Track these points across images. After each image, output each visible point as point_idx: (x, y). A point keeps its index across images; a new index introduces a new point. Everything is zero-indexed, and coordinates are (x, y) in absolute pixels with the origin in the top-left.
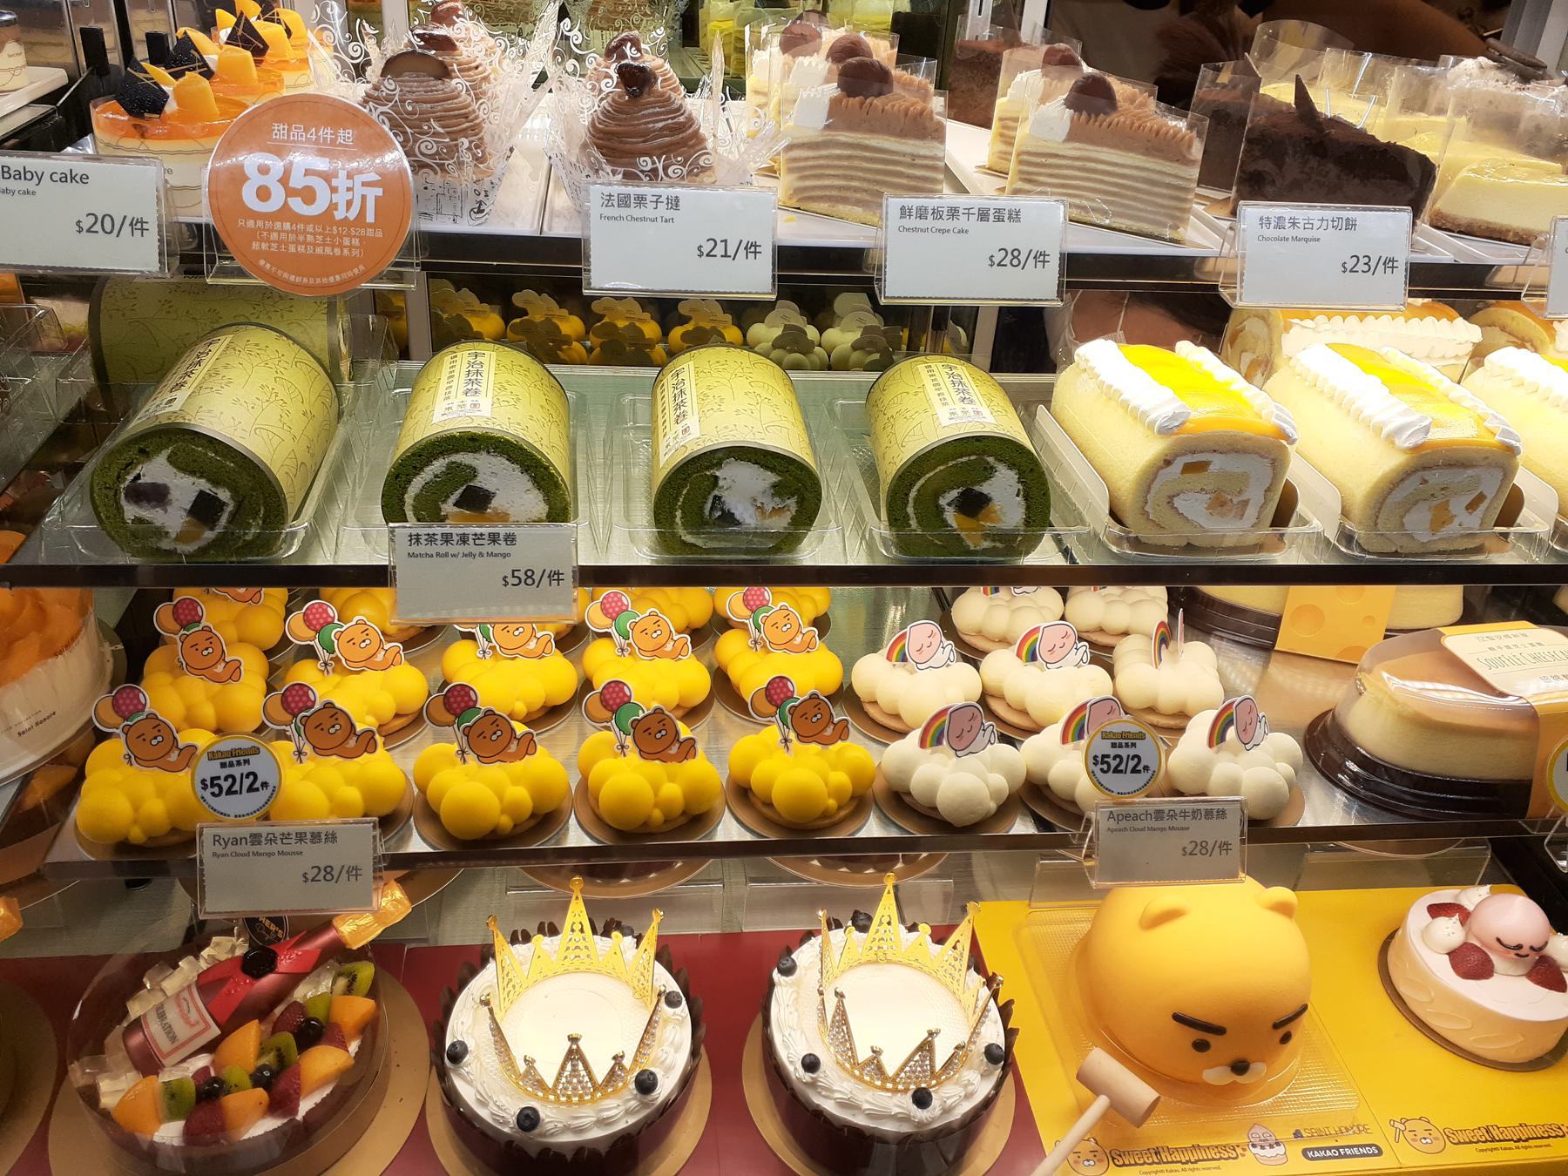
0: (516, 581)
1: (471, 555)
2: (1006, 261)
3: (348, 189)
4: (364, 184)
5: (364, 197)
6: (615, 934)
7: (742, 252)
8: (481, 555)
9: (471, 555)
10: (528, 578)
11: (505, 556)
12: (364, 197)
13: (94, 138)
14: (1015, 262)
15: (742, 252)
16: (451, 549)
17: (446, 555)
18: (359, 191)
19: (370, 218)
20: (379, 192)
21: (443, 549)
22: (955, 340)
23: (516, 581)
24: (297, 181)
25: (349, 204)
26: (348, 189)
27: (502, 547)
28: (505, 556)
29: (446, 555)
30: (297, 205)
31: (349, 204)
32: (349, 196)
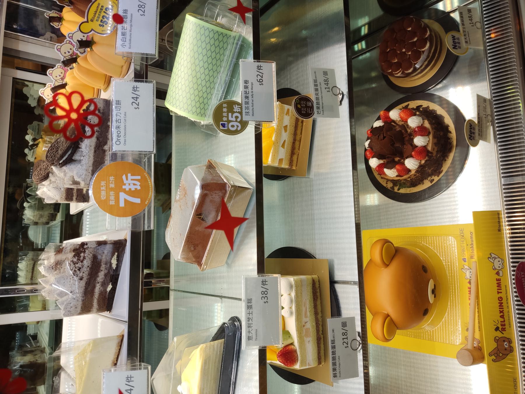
0: (266, 298)
1: (252, 95)
2: (143, 10)
3: (129, 185)
4: (127, 179)
5: (132, 180)
6: (415, 107)
7: (136, 93)
8: (252, 92)
9: (252, 95)
10: (265, 294)
11: (252, 84)
12: (132, 180)
13: (66, 372)
14: (143, 7)
15: (136, 93)
16: (250, 102)
17: (253, 103)
18: (129, 181)
19: (139, 177)
20: (129, 175)
21: (250, 105)
22: (99, 111)
23: (266, 298)
24: (234, 119)
25: (134, 184)
26: (129, 185)
27: (249, 85)
28: (252, 84)
29: (253, 103)
30: (239, 120)
31: (134, 184)
32: (132, 185)
